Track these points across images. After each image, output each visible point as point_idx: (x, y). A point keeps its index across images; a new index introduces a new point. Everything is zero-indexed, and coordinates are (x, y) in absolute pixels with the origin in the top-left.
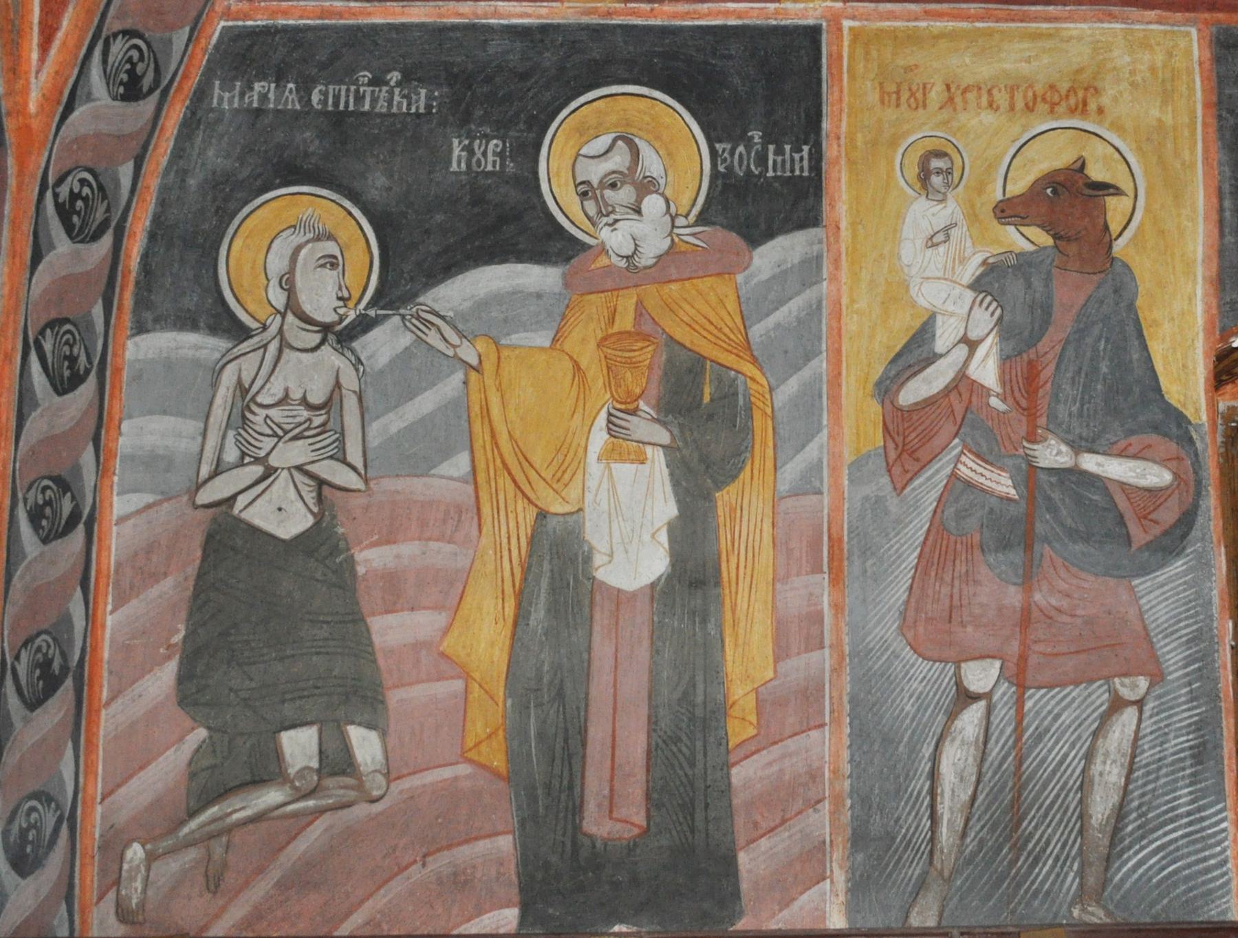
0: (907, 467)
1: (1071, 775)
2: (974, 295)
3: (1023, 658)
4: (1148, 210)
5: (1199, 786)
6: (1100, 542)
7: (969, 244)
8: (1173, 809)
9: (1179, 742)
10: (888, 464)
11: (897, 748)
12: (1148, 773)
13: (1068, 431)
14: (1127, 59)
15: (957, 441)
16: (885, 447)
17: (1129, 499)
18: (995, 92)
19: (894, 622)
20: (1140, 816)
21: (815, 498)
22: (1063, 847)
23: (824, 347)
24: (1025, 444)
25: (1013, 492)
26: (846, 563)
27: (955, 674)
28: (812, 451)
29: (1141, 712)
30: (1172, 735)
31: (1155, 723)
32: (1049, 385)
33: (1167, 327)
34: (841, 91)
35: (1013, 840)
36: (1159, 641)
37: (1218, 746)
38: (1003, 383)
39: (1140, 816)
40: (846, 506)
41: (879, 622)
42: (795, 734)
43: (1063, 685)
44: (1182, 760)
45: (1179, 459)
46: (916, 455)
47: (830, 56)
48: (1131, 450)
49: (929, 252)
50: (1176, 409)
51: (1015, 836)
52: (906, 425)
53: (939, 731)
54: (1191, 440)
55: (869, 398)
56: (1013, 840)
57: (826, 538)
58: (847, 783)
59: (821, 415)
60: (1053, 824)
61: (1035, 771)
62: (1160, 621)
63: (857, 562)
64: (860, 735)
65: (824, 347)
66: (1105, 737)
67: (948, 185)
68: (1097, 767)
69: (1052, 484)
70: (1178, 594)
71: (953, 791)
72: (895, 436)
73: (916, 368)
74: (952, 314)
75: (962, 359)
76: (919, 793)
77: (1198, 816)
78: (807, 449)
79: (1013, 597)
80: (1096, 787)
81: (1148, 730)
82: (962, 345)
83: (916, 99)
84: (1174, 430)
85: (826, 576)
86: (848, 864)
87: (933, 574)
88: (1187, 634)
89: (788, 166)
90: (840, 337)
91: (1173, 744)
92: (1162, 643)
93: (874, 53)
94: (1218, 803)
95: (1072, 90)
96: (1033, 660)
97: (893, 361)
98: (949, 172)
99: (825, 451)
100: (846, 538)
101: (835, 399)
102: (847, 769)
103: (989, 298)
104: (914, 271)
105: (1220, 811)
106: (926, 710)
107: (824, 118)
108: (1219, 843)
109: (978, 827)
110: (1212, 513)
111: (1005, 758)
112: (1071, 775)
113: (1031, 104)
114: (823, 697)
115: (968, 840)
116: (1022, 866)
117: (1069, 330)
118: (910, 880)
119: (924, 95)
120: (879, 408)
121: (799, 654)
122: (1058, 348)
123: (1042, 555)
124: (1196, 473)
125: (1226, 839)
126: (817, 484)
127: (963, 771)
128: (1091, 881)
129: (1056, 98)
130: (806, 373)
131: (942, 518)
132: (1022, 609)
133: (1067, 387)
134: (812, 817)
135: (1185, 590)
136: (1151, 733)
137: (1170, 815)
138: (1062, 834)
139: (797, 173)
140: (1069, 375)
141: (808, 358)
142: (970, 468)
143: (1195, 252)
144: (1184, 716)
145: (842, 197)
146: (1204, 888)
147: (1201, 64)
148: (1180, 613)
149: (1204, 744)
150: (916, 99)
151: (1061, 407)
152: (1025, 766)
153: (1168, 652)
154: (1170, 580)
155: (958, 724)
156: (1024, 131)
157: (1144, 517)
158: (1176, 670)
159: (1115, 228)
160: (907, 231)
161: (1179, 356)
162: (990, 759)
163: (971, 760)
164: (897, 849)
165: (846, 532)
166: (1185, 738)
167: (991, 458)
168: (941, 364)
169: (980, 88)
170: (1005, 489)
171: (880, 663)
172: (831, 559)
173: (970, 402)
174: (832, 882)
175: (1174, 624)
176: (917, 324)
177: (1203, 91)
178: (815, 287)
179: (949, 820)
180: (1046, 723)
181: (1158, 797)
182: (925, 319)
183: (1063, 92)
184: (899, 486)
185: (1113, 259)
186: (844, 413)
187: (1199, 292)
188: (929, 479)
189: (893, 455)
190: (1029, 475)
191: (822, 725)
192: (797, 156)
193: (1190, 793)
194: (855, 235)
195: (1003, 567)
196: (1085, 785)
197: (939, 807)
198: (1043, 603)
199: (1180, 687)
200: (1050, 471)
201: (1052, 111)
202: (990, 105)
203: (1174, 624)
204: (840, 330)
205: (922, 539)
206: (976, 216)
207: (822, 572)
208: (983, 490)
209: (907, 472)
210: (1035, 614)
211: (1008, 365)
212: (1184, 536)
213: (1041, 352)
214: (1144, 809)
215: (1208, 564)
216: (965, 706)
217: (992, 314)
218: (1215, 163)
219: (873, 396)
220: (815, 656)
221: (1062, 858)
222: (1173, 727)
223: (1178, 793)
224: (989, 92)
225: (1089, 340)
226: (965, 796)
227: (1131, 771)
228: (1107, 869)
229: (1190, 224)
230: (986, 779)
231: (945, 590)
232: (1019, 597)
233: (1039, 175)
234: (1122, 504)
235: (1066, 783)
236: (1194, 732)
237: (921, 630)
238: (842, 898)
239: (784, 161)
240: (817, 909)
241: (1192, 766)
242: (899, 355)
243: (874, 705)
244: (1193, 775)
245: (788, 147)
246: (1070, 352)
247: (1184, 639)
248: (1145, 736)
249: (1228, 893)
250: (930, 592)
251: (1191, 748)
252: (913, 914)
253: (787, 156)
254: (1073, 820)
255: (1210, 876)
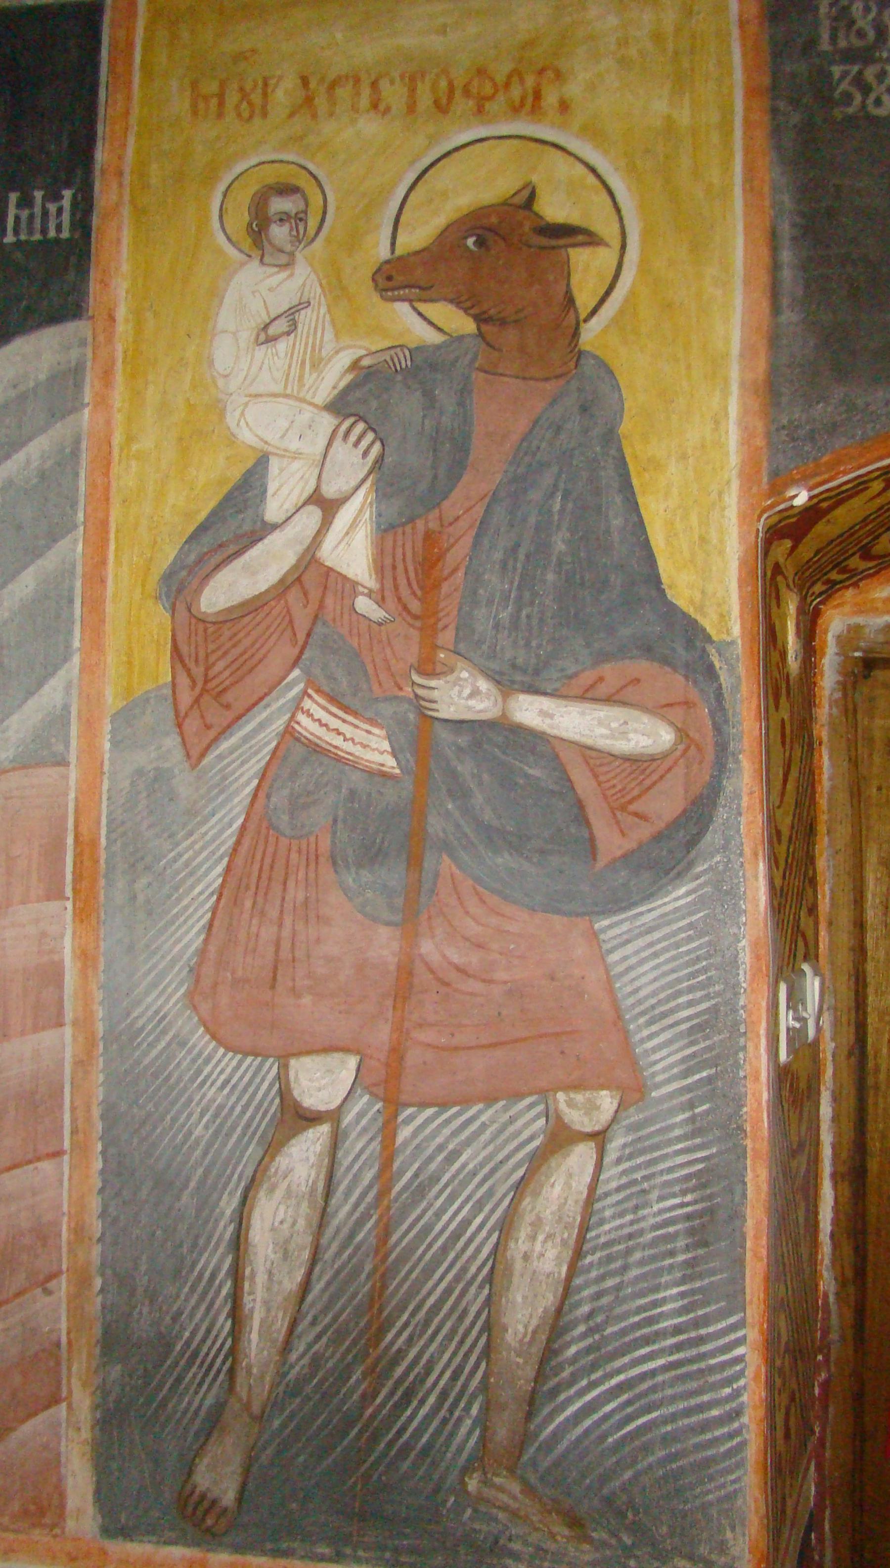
0: (209, 720)
1: (474, 1257)
2: (335, 422)
3: (397, 1054)
4: (644, 266)
5: (697, 1284)
6: (542, 852)
7: (329, 335)
8: (650, 1321)
9: (665, 1207)
10: (177, 715)
11: (178, 1199)
12: (610, 1259)
13: (492, 655)
14: (612, 21)
15: (296, 673)
16: (174, 684)
17: (596, 776)
18: (384, 84)
19: (181, 984)
20: (591, 1331)
21: (54, 772)
22: (455, 1377)
23: (81, 516)
24: (416, 678)
25: (390, 762)
26: (102, 882)
27: (278, 1077)
28: (52, 693)
29: (601, 1153)
30: (654, 1195)
31: (624, 1172)
32: (460, 574)
33: (673, 469)
34: (129, 98)
35: (369, 1361)
36: (640, 1028)
37: (737, 1215)
38: (379, 568)
39: (591, 1331)
40: (105, 786)
41: (154, 985)
42: (15, 1166)
43: (466, 1102)
44: (672, 1237)
45: (687, 704)
46: (229, 697)
47: (113, 45)
48: (602, 690)
49: (260, 352)
50: (685, 615)
51: (374, 1354)
52: (211, 647)
53: (249, 1172)
54: (711, 672)
55: (150, 603)
56: (369, 1361)
57: (70, 840)
58: (97, 1250)
59: (70, 632)
60: (440, 1337)
61: (411, 1249)
62: (642, 994)
63: (121, 884)
64: (119, 1174)
65: (81, 516)
66: (536, 1194)
67: (297, 239)
68: (519, 1245)
69: (460, 749)
70: (677, 945)
71: (270, 1274)
72: (191, 665)
73: (232, 549)
74: (296, 455)
75: (311, 532)
76: (213, 1276)
77: (693, 1334)
78: (46, 688)
79: (385, 945)
80: (516, 1280)
81: (614, 1184)
82: (311, 508)
83: (250, 103)
84: (681, 651)
85: (69, 905)
86: (98, 1381)
87: (248, 904)
88: (689, 1018)
89: (38, 224)
90: (107, 499)
91: (657, 1208)
92: (645, 1033)
93: (185, 35)
94: (730, 1314)
95: (516, 74)
96: (414, 1057)
97: (194, 537)
98: (300, 218)
99: (75, 692)
100: (103, 841)
101: (95, 605)
102: (96, 1227)
103: (361, 426)
104: (233, 386)
105: (734, 1328)
106: (228, 1135)
107: (99, 144)
108: (728, 1382)
109: (311, 1337)
110: (745, 801)
111: (360, 1223)
112: (474, 1257)
113: (444, 101)
114: (61, 1106)
115: (294, 1356)
116: (383, 1405)
117: (498, 478)
118: (196, 1413)
119: (265, 94)
120: (168, 616)
121: (23, 1033)
122: (479, 511)
123: (437, 875)
124: (717, 729)
125: (741, 1374)
126: (61, 748)
127: (287, 1241)
128: (501, 1433)
129: (488, 89)
130: (50, 561)
131: (267, 807)
132: (399, 967)
133: (492, 578)
134: (39, 1302)
135: (690, 939)
136: (618, 1189)
137: (646, 1331)
138: (455, 1353)
139: (52, 234)
140: (498, 556)
141: (53, 538)
142: (319, 721)
143: (727, 340)
144: (679, 1160)
145: (120, 274)
146: (700, 1456)
147: (742, 24)
148: (679, 981)
149: (711, 1211)
150: (250, 103)
151: (481, 613)
152: (394, 1238)
153: (654, 1050)
154: (664, 920)
155: (282, 1162)
156: (428, 147)
157: (621, 807)
158: (668, 1081)
159: (584, 299)
160: (226, 318)
161: (694, 520)
162: (335, 1222)
163: (301, 1223)
164: (176, 1364)
165: (104, 832)
166: (677, 1201)
167: (355, 704)
168: (274, 540)
169: (357, 80)
170: (376, 758)
171: (154, 1053)
172: (78, 877)
173: (321, 606)
174: (70, 1407)
175: (668, 999)
176: (236, 474)
177: (746, 69)
178: (70, 419)
179: (263, 1321)
180: (433, 1166)
181: (624, 1300)
182: (250, 464)
183: (500, 79)
184: (195, 753)
185: (580, 353)
186: (108, 627)
187: (734, 409)
188: (246, 739)
189: (186, 698)
190: (421, 733)
191: (58, 1154)
192: (52, 208)
193: (682, 1295)
194: (139, 328)
195: (369, 894)
196: (496, 1273)
197: (247, 1299)
198: (435, 958)
199: (672, 1112)
200: (459, 725)
201: (480, 110)
202: (375, 106)
203: (668, 999)
204: (107, 489)
205: (231, 842)
206: (344, 289)
207: (61, 896)
208: (339, 759)
209: (208, 727)
210: (422, 976)
211: (389, 543)
212: (692, 842)
213: (449, 515)
214: (599, 1319)
215: (732, 893)
216: (295, 1132)
217: (365, 454)
218: (766, 189)
219: (158, 598)
220: (48, 1037)
221: (453, 1395)
222: (659, 1180)
223: (661, 1295)
224: (374, 85)
225: (535, 495)
226: (291, 1282)
227: (578, 1253)
228: (529, 1416)
229: (719, 292)
230: (328, 1255)
231: (268, 933)
232: (395, 946)
233: (454, 216)
234: (584, 783)
235: (464, 1269)
236: (693, 1190)
237: (224, 1000)
238: (86, 1434)
239: (31, 217)
240: (46, 1447)
241: (687, 1248)
242: (203, 528)
243: (143, 1123)
244: (690, 1264)
245: (38, 195)
246: (500, 513)
247: (684, 1027)
248: (607, 1195)
249: (740, 1465)
250: (242, 936)
251: (688, 1217)
252: (202, 1465)
253: (38, 210)
254: (474, 1333)
255: (708, 1436)
